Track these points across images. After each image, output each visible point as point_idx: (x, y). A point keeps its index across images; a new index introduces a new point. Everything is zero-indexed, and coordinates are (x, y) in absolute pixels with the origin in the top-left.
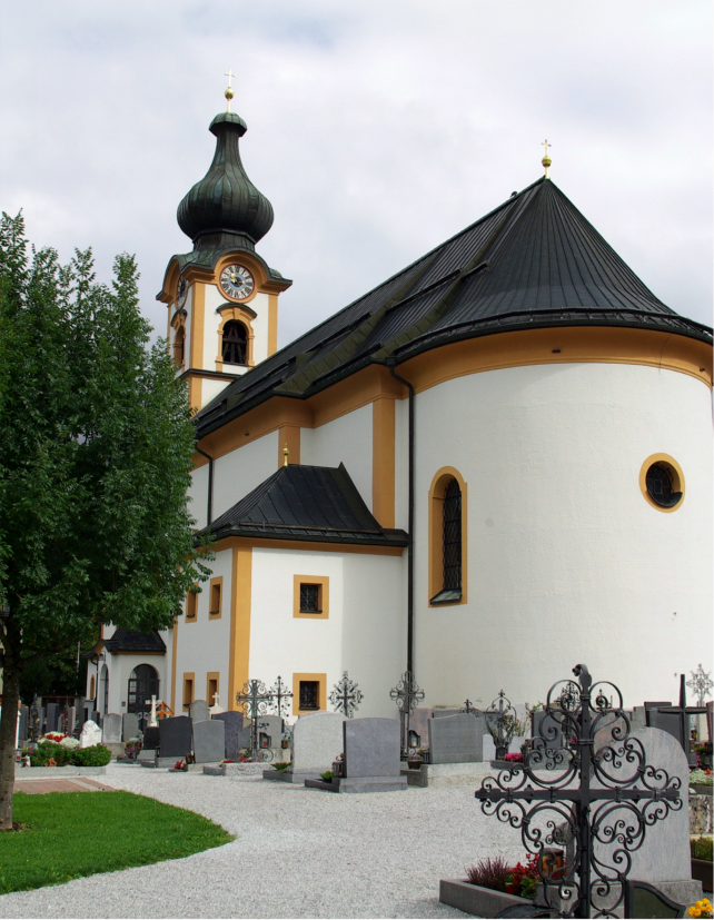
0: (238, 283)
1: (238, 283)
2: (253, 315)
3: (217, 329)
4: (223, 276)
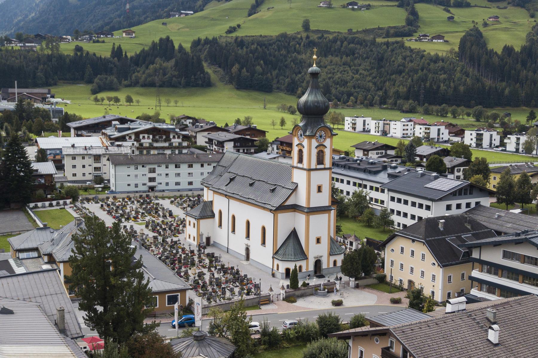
0: (321, 137)
1: (321, 137)
2: (326, 147)
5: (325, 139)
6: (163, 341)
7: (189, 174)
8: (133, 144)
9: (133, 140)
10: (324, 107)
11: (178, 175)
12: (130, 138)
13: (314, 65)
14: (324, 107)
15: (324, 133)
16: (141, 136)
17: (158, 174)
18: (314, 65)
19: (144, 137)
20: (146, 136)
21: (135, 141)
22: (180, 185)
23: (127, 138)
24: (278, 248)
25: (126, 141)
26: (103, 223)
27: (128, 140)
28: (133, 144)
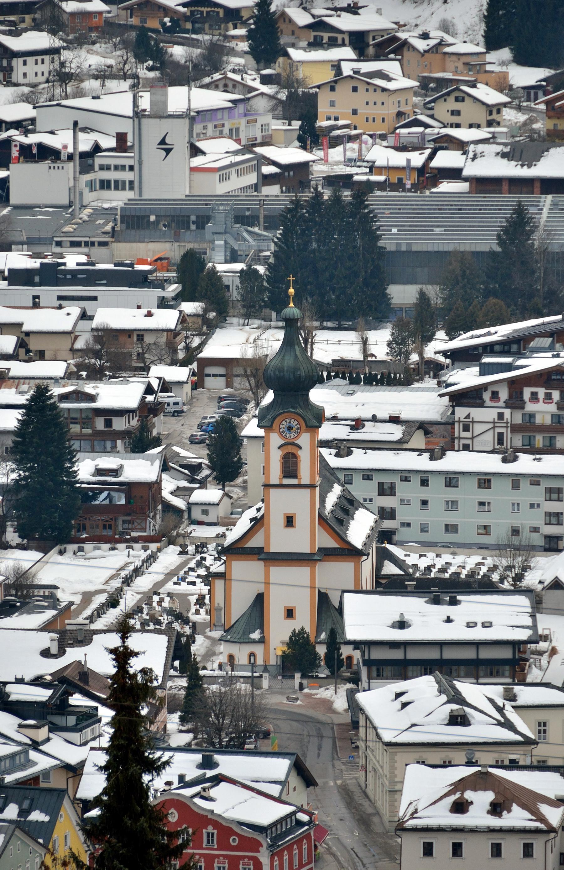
0: (290, 428)
1: (290, 428)
2: (300, 448)
3: (279, 458)
4: (281, 426)
5: (299, 434)
6: (9, 696)
7: (482, 504)
8: (501, 416)
9: (501, 404)
10: (292, 377)
11: (452, 505)
12: (495, 395)
13: (292, 305)
14: (292, 377)
15: (296, 423)
16: (527, 392)
17: (403, 500)
18: (292, 305)
19: (534, 396)
20: (541, 392)
21: (508, 405)
22: (456, 531)
23: (487, 396)
24: (232, 623)
25: (481, 405)
26: (441, 673)
27: (488, 403)
28: (501, 416)
